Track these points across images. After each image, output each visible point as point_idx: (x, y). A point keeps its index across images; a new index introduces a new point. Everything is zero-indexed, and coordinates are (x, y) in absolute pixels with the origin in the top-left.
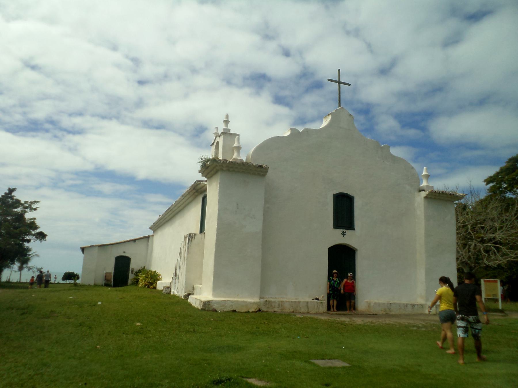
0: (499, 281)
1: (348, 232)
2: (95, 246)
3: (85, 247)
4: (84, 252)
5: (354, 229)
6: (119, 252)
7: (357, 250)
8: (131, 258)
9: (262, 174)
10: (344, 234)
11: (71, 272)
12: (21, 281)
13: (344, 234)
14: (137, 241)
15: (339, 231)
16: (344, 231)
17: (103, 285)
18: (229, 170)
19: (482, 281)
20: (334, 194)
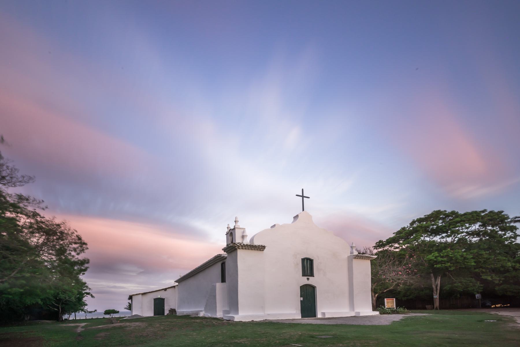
0: (394, 299)
1: (310, 278)
2: (139, 294)
3: (133, 295)
4: (294, 223)
5: (314, 276)
6: (159, 295)
7: (316, 287)
8: (313, 260)
9: (262, 249)
10: (308, 279)
11: (399, 231)
12: (77, 319)
13: (308, 279)
14: (167, 290)
15: (306, 278)
16: (308, 277)
17: (431, 301)
18: (243, 249)
19: (385, 299)
20: (302, 259)
